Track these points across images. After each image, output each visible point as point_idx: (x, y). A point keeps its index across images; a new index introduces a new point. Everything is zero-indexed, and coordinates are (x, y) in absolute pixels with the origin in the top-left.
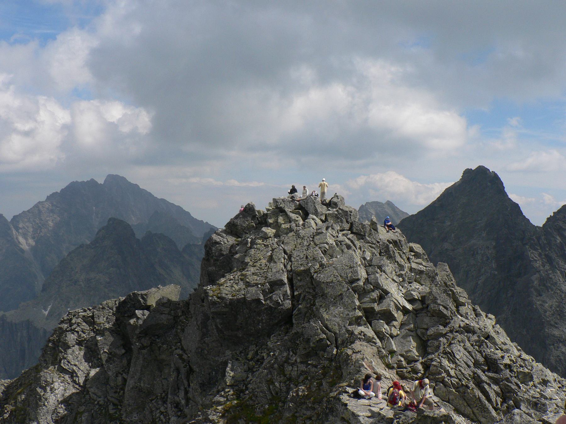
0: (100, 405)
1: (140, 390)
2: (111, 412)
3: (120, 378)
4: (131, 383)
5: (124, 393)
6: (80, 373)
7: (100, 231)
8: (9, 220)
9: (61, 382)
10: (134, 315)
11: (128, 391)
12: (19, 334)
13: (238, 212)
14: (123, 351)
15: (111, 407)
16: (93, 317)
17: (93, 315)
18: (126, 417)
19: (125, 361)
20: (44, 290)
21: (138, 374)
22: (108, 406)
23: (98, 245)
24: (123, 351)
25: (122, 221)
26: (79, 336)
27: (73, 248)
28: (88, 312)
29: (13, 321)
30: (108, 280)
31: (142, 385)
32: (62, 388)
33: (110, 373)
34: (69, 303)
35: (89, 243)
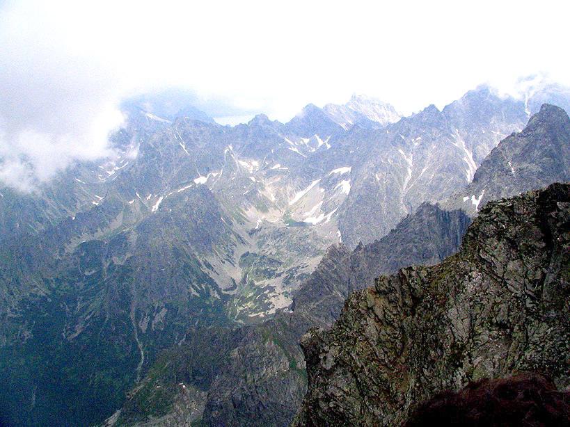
0: (517, 298)
1: (559, 287)
2: (529, 306)
3: (539, 273)
4: (550, 278)
5: (542, 288)
6: (498, 265)
7: (532, 118)
8: (441, 110)
9: (479, 272)
10: (555, 207)
11: (546, 286)
12: (452, 222)
13: (284, 111)
14: (544, 245)
15: (529, 301)
16: (512, 208)
17: (513, 206)
18: (543, 313)
19: (544, 256)
20: (475, 180)
21: (558, 270)
22: (525, 300)
23: (530, 133)
24: (544, 245)
25: (556, 106)
26: (497, 226)
27: (504, 137)
28: (508, 202)
29: (447, 210)
30: (541, 170)
31: (562, 281)
32: (479, 277)
33: (529, 266)
34: (500, 193)
35: (521, 131)
